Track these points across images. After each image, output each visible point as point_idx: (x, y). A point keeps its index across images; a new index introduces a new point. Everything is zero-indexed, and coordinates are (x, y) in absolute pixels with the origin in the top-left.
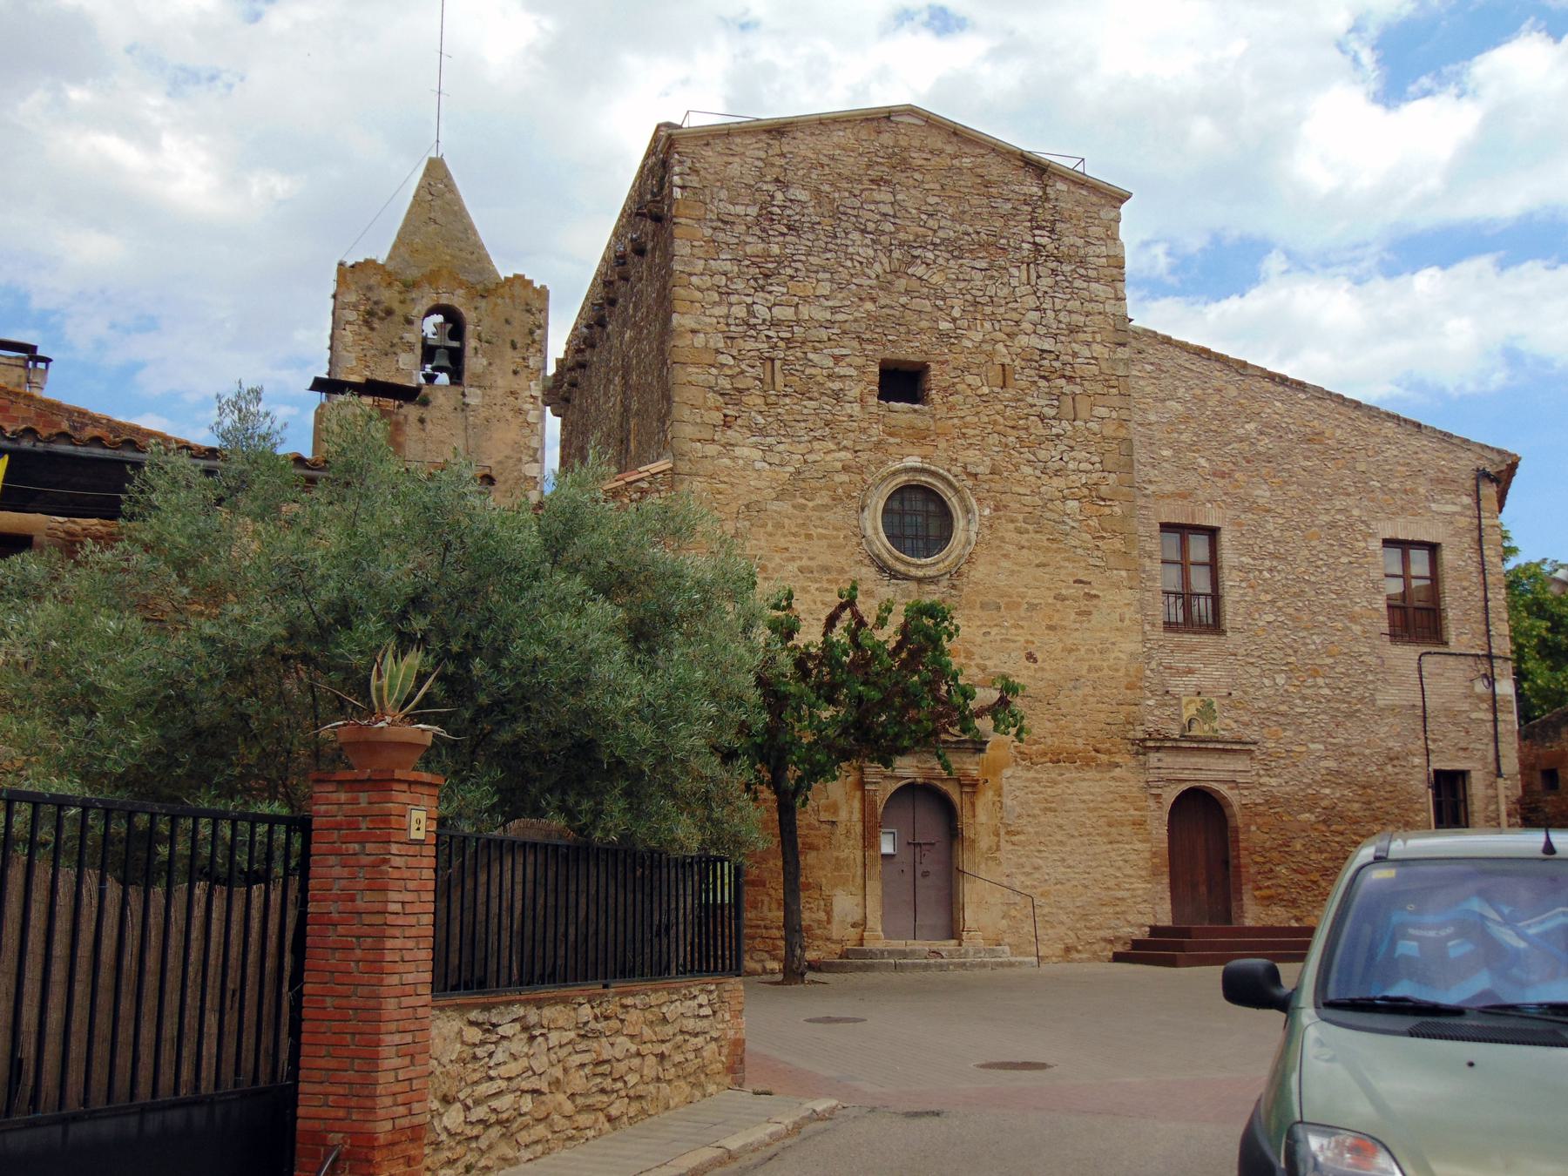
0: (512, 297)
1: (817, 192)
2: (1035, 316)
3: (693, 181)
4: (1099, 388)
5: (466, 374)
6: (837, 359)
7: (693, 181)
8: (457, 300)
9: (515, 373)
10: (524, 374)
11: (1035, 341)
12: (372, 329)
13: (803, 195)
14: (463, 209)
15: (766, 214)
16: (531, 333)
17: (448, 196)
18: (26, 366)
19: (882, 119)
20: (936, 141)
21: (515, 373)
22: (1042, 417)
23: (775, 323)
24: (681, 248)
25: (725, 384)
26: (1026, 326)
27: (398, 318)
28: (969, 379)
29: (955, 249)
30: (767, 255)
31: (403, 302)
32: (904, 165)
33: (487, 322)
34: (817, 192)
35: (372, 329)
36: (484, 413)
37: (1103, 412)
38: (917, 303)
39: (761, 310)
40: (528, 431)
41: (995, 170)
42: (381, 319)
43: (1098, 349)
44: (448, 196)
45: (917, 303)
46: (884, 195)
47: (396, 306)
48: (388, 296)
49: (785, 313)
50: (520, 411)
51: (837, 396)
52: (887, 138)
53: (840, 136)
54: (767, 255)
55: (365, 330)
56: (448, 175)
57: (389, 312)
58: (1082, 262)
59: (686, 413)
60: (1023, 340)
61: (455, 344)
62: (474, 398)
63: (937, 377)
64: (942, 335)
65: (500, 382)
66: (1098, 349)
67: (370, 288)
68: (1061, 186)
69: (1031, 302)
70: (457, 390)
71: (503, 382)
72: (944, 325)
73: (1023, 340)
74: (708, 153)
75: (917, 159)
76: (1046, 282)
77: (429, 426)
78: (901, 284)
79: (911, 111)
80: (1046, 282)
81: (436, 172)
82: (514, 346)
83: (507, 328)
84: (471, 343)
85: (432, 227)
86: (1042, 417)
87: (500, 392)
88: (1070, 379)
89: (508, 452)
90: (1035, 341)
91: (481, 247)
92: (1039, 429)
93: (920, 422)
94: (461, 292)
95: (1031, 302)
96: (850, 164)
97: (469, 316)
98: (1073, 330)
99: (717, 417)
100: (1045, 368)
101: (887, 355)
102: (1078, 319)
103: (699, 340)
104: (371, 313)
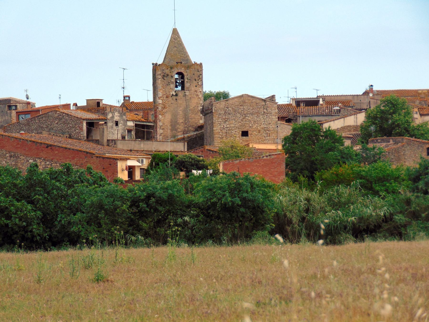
0: (194, 68)
1: (232, 108)
2: (264, 122)
3: (216, 109)
4: (273, 132)
5: (185, 88)
6: (236, 132)
7: (216, 109)
8: (182, 70)
9: (196, 86)
10: (198, 87)
11: (264, 126)
12: (164, 79)
13: (230, 109)
14: (182, 42)
15: (225, 112)
16: (199, 76)
17: (178, 39)
18: (194, 194)
19: (242, 96)
20: (249, 98)
21: (196, 86)
22: (265, 137)
23: (227, 128)
24: (214, 119)
25: (221, 137)
26: (262, 124)
27: (170, 76)
28: (255, 132)
29: (252, 114)
30: (226, 118)
31: (170, 72)
32: (245, 102)
33: (189, 75)
34: (232, 108)
35: (164, 79)
36: (190, 96)
37: (273, 135)
38: (247, 122)
39: (225, 126)
40: (199, 100)
41: (258, 101)
42: (166, 77)
43: (273, 126)
44: (178, 39)
45: (247, 122)
46: (242, 107)
47: (169, 73)
48: (167, 71)
49: (228, 126)
50: (197, 95)
51: (235, 137)
52: (242, 99)
53: (236, 100)
54: (226, 118)
55: (163, 80)
56: (178, 33)
57: (168, 75)
58: (271, 114)
59: (215, 141)
60: (262, 126)
61: (182, 80)
62: (187, 93)
63: (249, 133)
64: (250, 127)
65: (193, 89)
66: (273, 126)
67: (163, 70)
68: (268, 102)
69: (263, 120)
70: (183, 91)
71: (193, 89)
72: (251, 125)
73: (262, 126)
74: (217, 105)
75: (247, 101)
76: (265, 117)
77: (178, 101)
78: (244, 120)
79: (246, 95)
80: (265, 117)
81: (175, 32)
82: (195, 80)
83: (194, 76)
84: (186, 80)
85: (175, 48)
86: (265, 137)
87: (193, 91)
88: (269, 131)
89: (195, 105)
90: (264, 126)
91: (187, 53)
92: (264, 138)
93: (247, 139)
94: (183, 68)
95: (263, 120)
96: (237, 103)
97: (185, 74)
98: (270, 124)
99: (220, 141)
100: (266, 130)
101: (243, 130)
102: (270, 122)
103: (217, 131)
104: (164, 76)
